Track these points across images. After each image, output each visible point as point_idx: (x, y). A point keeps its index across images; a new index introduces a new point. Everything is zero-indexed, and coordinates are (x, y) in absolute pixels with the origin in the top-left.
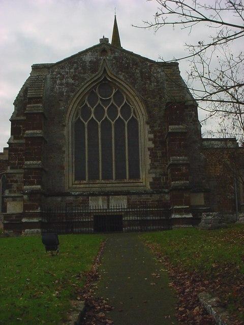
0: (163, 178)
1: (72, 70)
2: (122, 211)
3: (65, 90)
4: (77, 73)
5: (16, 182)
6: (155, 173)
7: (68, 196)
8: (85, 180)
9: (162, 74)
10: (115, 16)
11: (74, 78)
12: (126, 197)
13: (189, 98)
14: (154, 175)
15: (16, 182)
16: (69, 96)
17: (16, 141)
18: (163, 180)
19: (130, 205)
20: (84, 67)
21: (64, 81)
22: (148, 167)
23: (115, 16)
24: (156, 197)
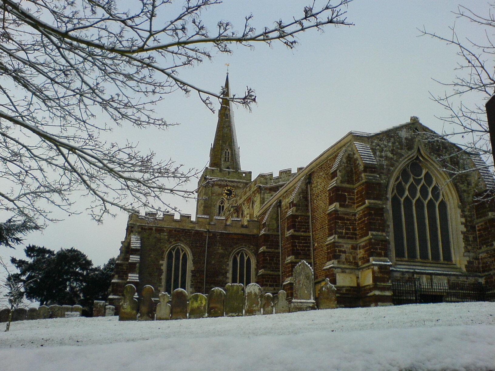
0: (476, 262)
1: (390, 144)
3: (385, 163)
4: (395, 148)
5: (344, 252)
6: (469, 256)
10: (228, 73)
11: (392, 152)
15: (344, 252)
16: (389, 170)
20: (400, 143)
21: (383, 154)
22: (463, 250)
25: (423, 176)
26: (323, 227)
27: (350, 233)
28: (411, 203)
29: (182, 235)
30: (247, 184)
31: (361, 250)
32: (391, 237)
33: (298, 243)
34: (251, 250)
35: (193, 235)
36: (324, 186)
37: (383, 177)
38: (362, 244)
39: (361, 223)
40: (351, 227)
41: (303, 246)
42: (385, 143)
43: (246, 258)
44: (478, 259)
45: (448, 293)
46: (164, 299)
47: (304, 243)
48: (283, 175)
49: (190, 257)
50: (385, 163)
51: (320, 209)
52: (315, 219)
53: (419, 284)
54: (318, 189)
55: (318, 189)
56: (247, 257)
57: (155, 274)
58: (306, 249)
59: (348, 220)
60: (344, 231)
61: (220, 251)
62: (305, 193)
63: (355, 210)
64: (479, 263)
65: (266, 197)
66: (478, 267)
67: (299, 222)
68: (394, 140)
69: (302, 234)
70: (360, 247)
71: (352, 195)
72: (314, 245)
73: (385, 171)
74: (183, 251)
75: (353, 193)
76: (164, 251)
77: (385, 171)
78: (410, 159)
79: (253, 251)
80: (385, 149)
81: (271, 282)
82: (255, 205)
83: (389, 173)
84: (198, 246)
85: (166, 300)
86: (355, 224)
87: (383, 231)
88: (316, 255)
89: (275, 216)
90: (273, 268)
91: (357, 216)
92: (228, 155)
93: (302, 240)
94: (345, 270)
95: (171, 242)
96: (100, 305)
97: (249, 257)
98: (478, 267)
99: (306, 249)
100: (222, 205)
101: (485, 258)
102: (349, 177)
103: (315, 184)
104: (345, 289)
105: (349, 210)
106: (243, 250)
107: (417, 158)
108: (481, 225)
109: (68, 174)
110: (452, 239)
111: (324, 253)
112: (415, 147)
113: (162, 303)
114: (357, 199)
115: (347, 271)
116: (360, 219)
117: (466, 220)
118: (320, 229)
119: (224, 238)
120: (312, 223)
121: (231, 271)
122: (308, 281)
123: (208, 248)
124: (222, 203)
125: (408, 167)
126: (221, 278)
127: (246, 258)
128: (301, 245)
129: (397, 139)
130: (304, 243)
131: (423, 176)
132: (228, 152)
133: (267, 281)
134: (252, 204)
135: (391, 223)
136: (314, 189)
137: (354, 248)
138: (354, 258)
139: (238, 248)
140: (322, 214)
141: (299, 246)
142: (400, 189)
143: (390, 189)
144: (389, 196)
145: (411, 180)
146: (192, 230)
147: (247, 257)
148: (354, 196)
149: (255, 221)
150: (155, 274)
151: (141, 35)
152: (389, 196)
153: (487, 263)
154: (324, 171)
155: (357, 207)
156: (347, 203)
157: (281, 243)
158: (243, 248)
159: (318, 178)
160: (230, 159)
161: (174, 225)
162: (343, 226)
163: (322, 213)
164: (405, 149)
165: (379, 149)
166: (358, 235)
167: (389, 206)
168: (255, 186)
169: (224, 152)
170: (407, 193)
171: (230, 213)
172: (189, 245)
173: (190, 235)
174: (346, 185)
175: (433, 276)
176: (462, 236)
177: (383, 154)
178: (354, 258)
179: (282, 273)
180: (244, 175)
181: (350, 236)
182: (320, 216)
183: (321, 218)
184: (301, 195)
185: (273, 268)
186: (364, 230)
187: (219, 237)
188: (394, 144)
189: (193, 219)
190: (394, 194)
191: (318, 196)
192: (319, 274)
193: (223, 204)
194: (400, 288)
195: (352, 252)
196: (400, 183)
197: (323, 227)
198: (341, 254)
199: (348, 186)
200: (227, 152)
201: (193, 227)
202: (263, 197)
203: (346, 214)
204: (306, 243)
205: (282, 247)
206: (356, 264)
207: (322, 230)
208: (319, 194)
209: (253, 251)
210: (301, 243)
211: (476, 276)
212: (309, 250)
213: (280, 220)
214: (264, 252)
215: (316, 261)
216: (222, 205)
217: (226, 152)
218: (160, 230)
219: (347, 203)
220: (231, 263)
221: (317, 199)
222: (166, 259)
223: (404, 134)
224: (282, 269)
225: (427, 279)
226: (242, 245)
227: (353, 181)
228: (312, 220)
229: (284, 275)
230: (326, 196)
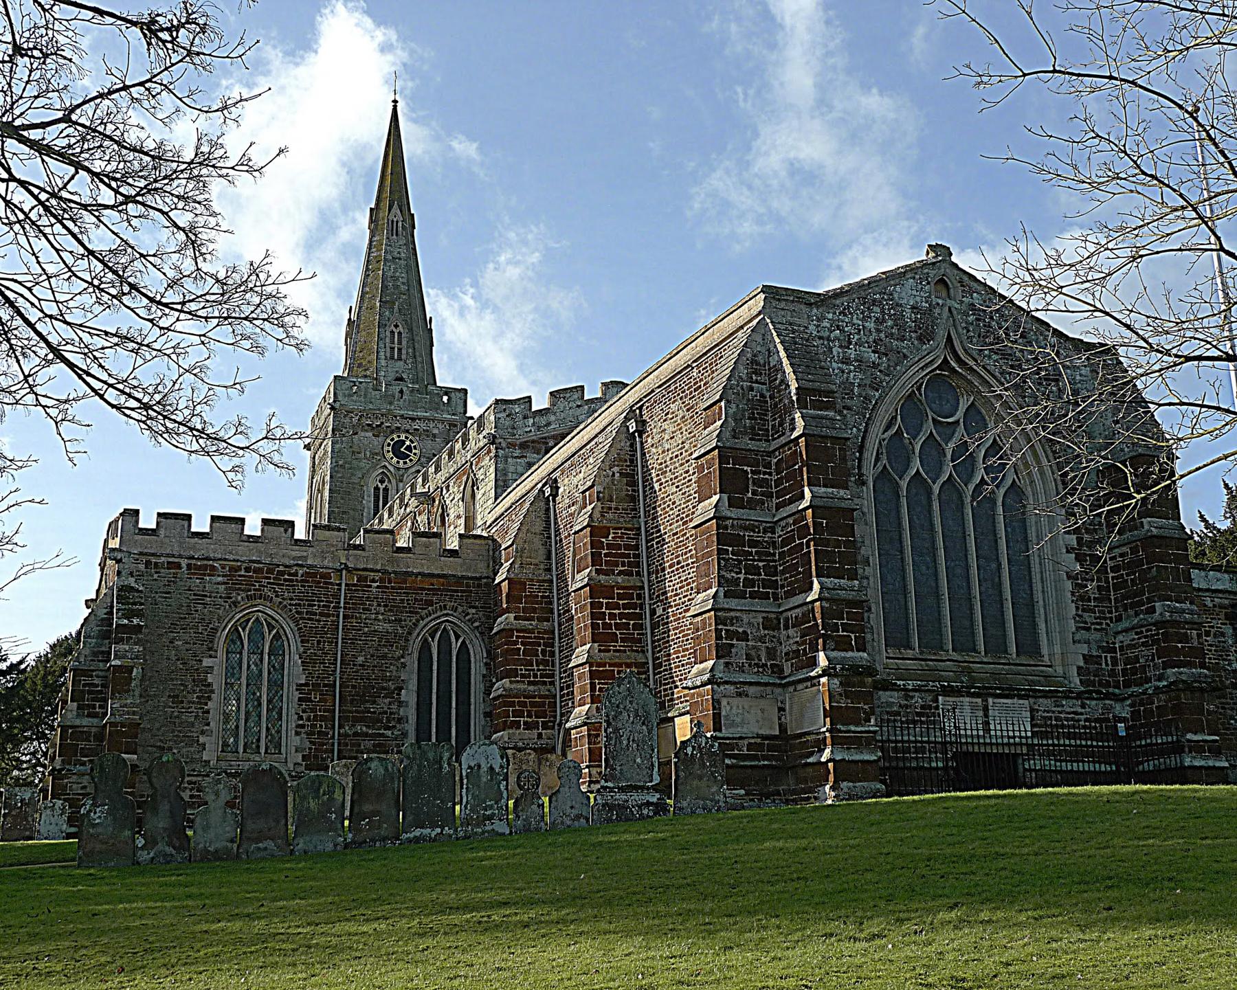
0: (1106, 657)
1: (871, 325)
2: (1021, 744)
3: (855, 378)
4: (882, 335)
5: (744, 637)
6: (1088, 642)
7: (886, 689)
8: (909, 646)
9: (1083, 372)
10: (395, 101)
11: (876, 346)
12: (1026, 702)
13: (93, 624)
14: (1084, 649)
15: (744, 637)
16: (867, 399)
17: (734, 513)
18: (1107, 665)
19: (1042, 728)
20: (898, 320)
21: (852, 353)
22: (1072, 626)
23: (395, 101)
24: (1095, 707)
25: (960, 414)
26: (679, 563)
27: (758, 580)
28: (929, 492)
29: (268, 583)
30: (452, 425)
31: (791, 632)
32: (874, 594)
33: (608, 606)
34: (469, 620)
35: (302, 581)
36: (683, 443)
37: (851, 418)
38: (794, 613)
39: (790, 552)
40: (761, 564)
41: (621, 616)
42: (855, 321)
43: (455, 646)
44: (1114, 650)
45: (1031, 747)
46: (217, 794)
47: (625, 606)
48: (561, 404)
49: (294, 646)
50: (855, 378)
51: (672, 509)
52: (657, 537)
53: (955, 727)
54: (663, 452)
55: (663, 452)
56: (460, 641)
57: (190, 697)
58: (632, 622)
59: (753, 544)
60: (742, 576)
61: (382, 627)
62: (626, 461)
63: (774, 516)
64: (1115, 662)
65: (512, 469)
66: (1113, 673)
67: (609, 546)
68: (883, 312)
69: (619, 579)
70: (787, 619)
71: (765, 473)
72: (653, 612)
73: (855, 403)
74: (271, 627)
75: (768, 465)
76: (215, 630)
77: (855, 403)
78: (926, 366)
79: (476, 624)
80: (857, 337)
81: (529, 716)
82: (482, 492)
83: (868, 411)
84: (315, 614)
85: (225, 796)
86: (774, 555)
87: (853, 576)
88: (659, 640)
89: (539, 526)
90: (535, 676)
91: (779, 531)
92: (400, 343)
93: (620, 597)
94: (746, 688)
95: (235, 604)
96: (22, 801)
97: (464, 642)
98: (1113, 673)
99: (632, 622)
100: (381, 487)
101: (1130, 646)
102: (755, 419)
103: (657, 437)
104: (746, 742)
105: (753, 515)
106: (447, 621)
107: (945, 361)
108: (1122, 555)
109: (15, 201)
110: (1040, 595)
111: (683, 636)
112: (941, 335)
113: (212, 805)
114: (778, 483)
115: (752, 690)
116: (785, 542)
117: (1079, 540)
118: (671, 566)
119: (393, 588)
120: (648, 548)
121: (413, 685)
122: (644, 727)
123: (345, 617)
124: (382, 482)
125: (919, 389)
126: (383, 703)
127: (455, 646)
128: (617, 611)
129: (889, 309)
130: (625, 606)
131: (960, 414)
132: (400, 333)
133: (518, 714)
134: (473, 486)
135: (870, 549)
136: (654, 450)
137: (771, 624)
138: (771, 653)
139: (433, 616)
140: (675, 525)
141: (612, 616)
142: (897, 450)
143: (870, 455)
144: (870, 473)
145: (929, 427)
146: (297, 565)
147: (460, 641)
148: (770, 474)
149: (480, 537)
150: (190, 697)
151: (19, 280)
152: (870, 473)
153: (1137, 659)
154: (681, 399)
155: (778, 507)
156: (750, 495)
157: (559, 605)
158: (447, 615)
159: (665, 421)
160: (404, 352)
161: (245, 553)
162: (740, 562)
163: (677, 521)
164: (911, 337)
165: (837, 338)
166: (783, 586)
167: (866, 500)
168: (481, 436)
169: (388, 334)
170: (916, 465)
171: (408, 510)
172: (291, 610)
173: (292, 581)
174: (746, 443)
175: (990, 700)
176: (1069, 585)
177: (852, 353)
178: (771, 653)
179: (562, 689)
180: (445, 399)
181: (758, 591)
182: (671, 530)
183: (674, 535)
184: (616, 469)
185: (535, 676)
186: (800, 573)
187: (378, 587)
188: (881, 323)
189: (300, 533)
190: (880, 468)
191: (666, 472)
192: (667, 695)
193: (386, 483)
194: (902, 736)
195: (765, 635)
196: (899, 433)
197: (679, 563)
198: (734, 642)
199: (752, 445)
200: (396, 331)
201: (300, 558)
202: (504, 469)
203: (746, 529)
204: (634, 606)
205: (559, 615)
206: (778, 670)
207: (677, 569)
208: (666, 467)
209: (476, 624)
210: (617, 606)
211: (1108, 696)
212: (639, 627)
213: (553, 537)
214: (507, 632)
215: (658, 658)
216: (381, 487)
217: (392, 332)
218: (202, 568)
219: (750, 495)
220: (412, 662)
221: (663, 480)
222: (221, 653)
223: (908, 295)
224: (561, 678)
225: (974, 708)
226: (445, 609)
227: (767, 430)
228: (647, 542)
229: (568, 694)
230: (687, 472)
